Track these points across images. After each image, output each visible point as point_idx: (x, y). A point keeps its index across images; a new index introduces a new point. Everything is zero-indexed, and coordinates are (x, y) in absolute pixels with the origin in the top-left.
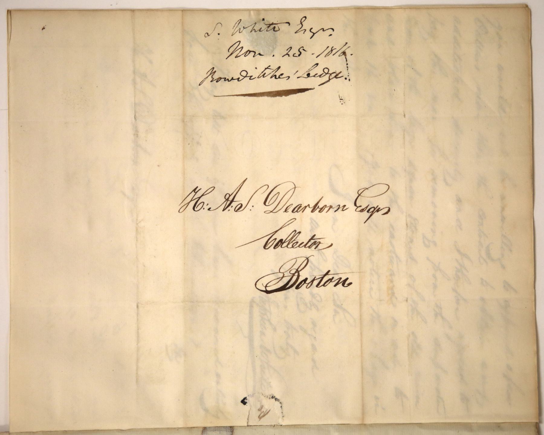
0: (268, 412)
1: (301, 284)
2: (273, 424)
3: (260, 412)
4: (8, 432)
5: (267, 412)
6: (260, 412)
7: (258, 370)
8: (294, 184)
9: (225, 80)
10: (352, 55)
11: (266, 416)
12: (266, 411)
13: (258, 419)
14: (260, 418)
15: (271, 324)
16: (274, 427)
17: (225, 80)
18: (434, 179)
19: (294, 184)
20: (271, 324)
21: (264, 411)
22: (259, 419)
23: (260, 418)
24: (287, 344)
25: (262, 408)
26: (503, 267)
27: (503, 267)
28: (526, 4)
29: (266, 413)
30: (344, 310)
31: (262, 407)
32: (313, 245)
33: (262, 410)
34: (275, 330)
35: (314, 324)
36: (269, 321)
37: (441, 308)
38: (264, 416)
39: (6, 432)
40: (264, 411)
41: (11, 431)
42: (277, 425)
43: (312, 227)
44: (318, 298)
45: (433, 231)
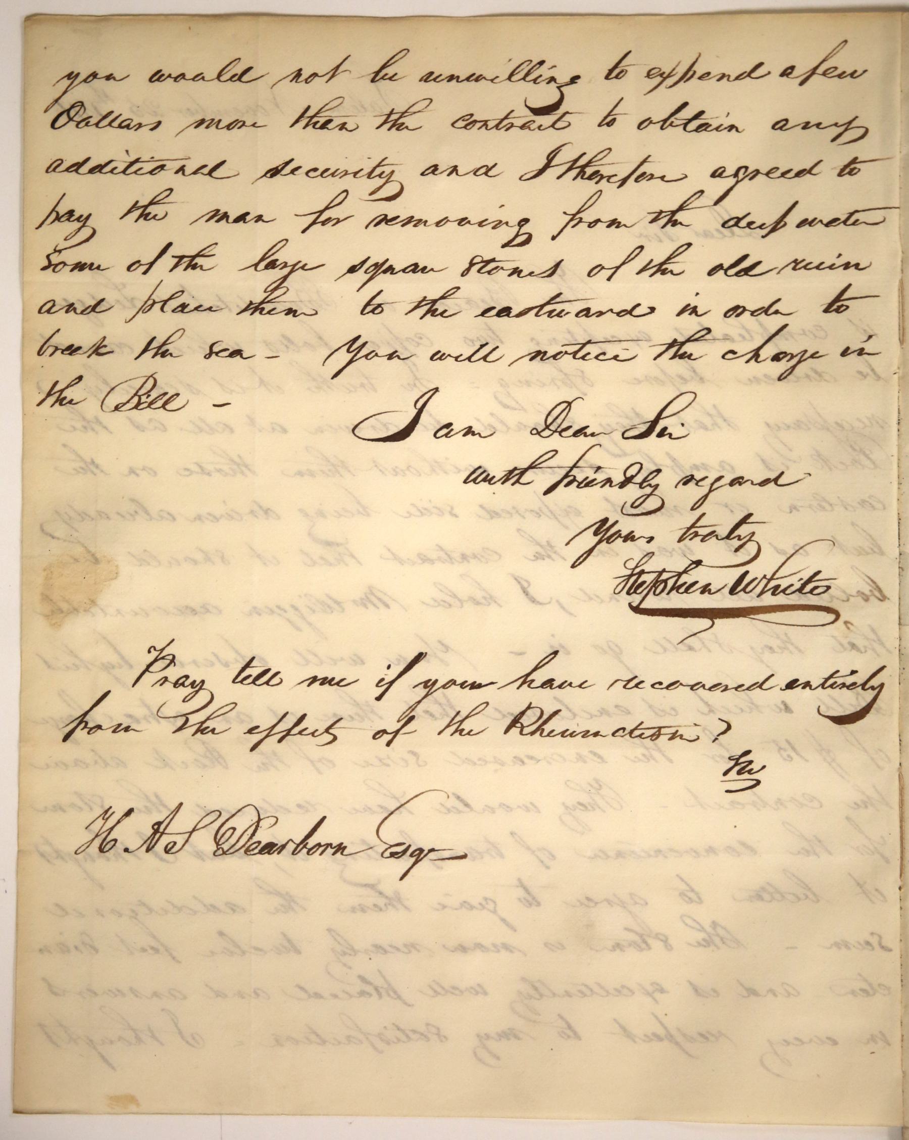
0: (872, 581)
1: (740, 585)
2: (897, 570)
3: (872, 599)
4: (904, 1128)
5: (871, 583)
6: (872, 599)
7: (781, 599)
8: (326, 360)
9: (458, 77)
10: (837, 255)
11: (881, 585)
12: (871, 586)
13: (886, 604)
14: (883, 598)
15: (685, 571)
16: (903, 570)
17: (458, 77)
18: (386, 220)
19: (326, 360)
20: (685, 571)
21: (870, 588)
22: (887, 600)
23: (883, 598)
24: (728, 537)
25: (863, 593)
26: (574, 80)
27: (574, 80)
28: (23, 19)
29: (873, 585)
30: (658, 417)
31: (860, 593)
32: (616, 539)
33: (868, 593)
34: (698, 563)
35: (688, 480)
36: (679, 575)
37: (661, 212)
38: (880, 590)
39: (903, 1134)
40: (870, 588)
41: (898, 1123)
42: (900, 562)
43: (484, 480)
44: (632, 471)
45: (498, 224)
